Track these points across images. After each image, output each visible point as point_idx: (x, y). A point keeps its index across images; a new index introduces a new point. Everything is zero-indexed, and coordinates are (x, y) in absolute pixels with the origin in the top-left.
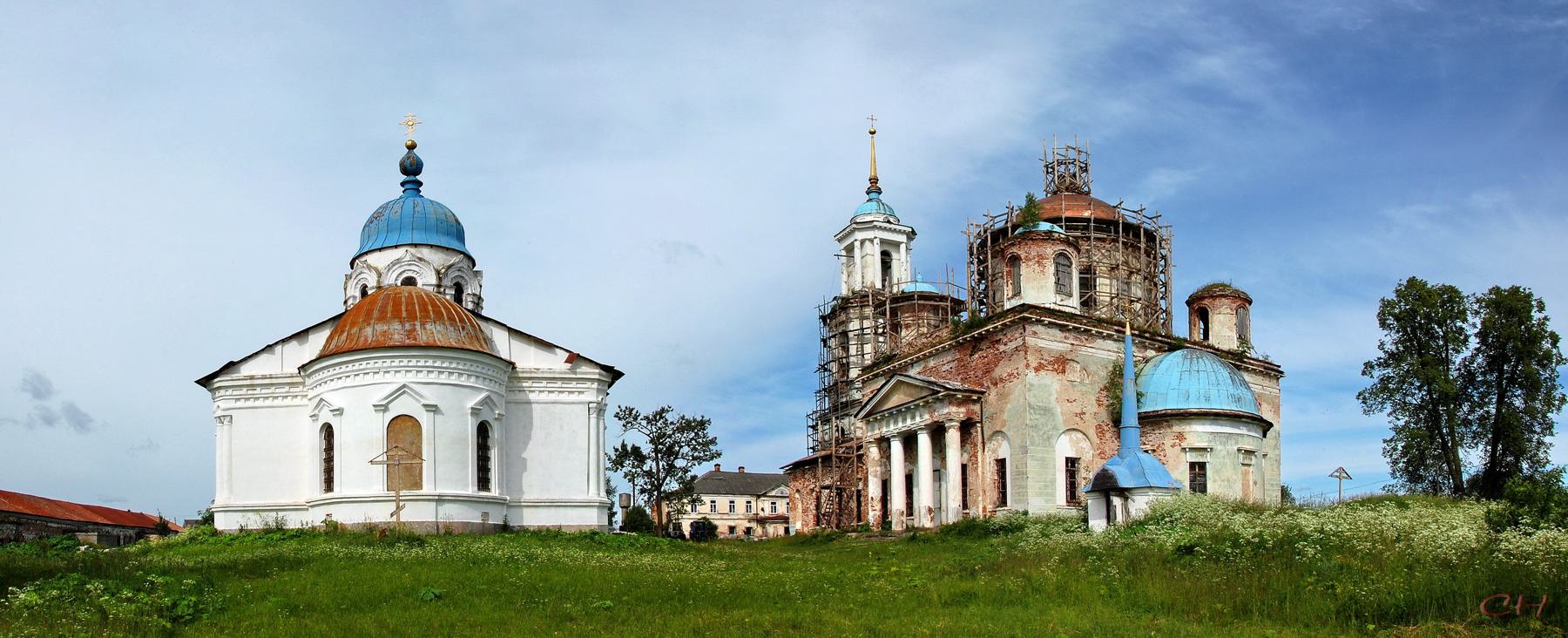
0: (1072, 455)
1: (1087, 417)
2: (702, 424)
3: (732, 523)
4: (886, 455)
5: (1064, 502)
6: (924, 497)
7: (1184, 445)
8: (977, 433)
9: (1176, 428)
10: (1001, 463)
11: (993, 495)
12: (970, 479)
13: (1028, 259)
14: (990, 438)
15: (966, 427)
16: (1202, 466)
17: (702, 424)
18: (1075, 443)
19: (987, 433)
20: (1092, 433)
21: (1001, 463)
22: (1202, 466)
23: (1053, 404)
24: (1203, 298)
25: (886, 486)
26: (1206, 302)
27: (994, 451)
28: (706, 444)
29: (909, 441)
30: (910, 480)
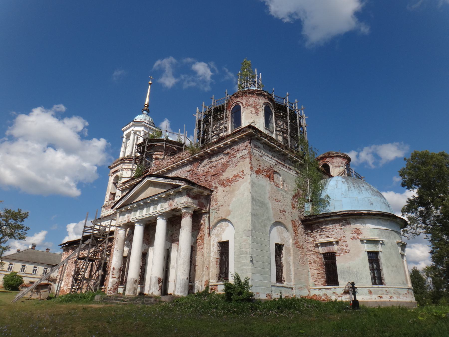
0: (279, 242)
1: (286, 214)
2: (24, 217)
3: (32, 280)
4: (129, 239)
5: (275, 282)
6: (154, 270)
7: (361, 237)
8: (204, 221)
9: (353, 226)
10: (224, 246)
11: (214, 270)
12: (199, 258)
13: (247, 105)
14: (215, 226)
15: (197, 217)
16: (377, 253)
17: (24, 217)
18: (280, 233)
19: (213, 222)
20: (290, 226)
21: (224, 246)
22: (377, 253)
23: (267, 201)
24: (326, 157)
25: (125, 259)
26: (328, 160)
27: (218, 235)
28: (19, 227)
29: (149, 227)
30: (144, 256)
